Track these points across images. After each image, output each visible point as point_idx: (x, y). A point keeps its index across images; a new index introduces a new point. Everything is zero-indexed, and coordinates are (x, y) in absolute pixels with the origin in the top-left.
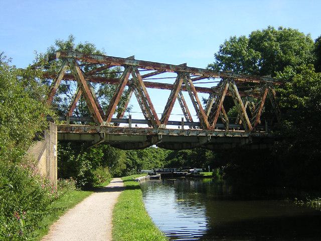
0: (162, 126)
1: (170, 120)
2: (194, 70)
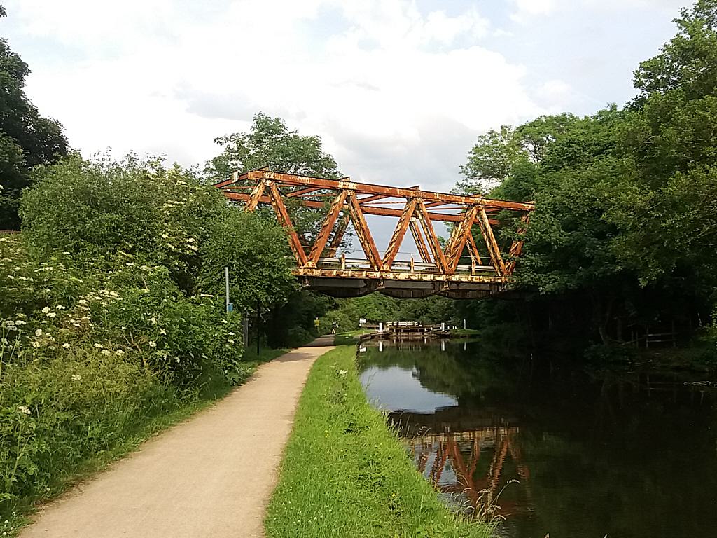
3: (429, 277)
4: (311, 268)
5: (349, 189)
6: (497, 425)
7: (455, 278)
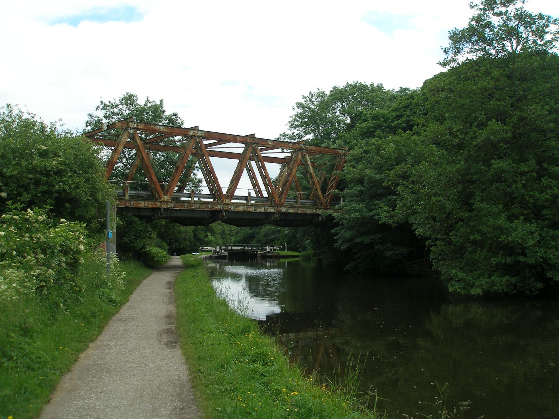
0: (227, 201)
1: (236, 194)
2: (264, 141)
3: (262, 210)
4: (166, 202)
5: (198, 136)
6: (315, 327)
7: (283, 210)
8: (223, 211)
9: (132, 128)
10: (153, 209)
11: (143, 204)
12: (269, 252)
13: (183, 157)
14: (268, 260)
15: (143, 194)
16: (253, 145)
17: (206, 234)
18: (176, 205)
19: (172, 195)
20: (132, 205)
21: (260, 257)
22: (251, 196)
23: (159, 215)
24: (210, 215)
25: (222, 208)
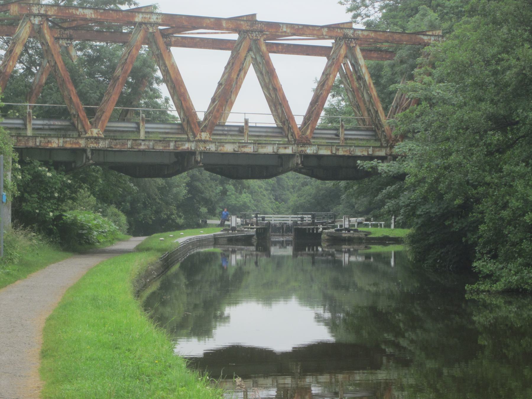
4: (95, 138)
5: (150, 24)
7: (310, 150)
8: (197, 153)
9: (38, 15)
10: (74, 151)
11: (55, 143)
12: (346, 229)
13: (126, 60)
14: (345, 247)
15: (57, 125)
16: (252, 34)
17: (224, 188)
18: (113, 143)
19: (107, 127)
20: (38, 144)
21: (328, 240)
22: (250, 125)
23: (84, 161)
24: (176, 160)
25: (193, 148)
